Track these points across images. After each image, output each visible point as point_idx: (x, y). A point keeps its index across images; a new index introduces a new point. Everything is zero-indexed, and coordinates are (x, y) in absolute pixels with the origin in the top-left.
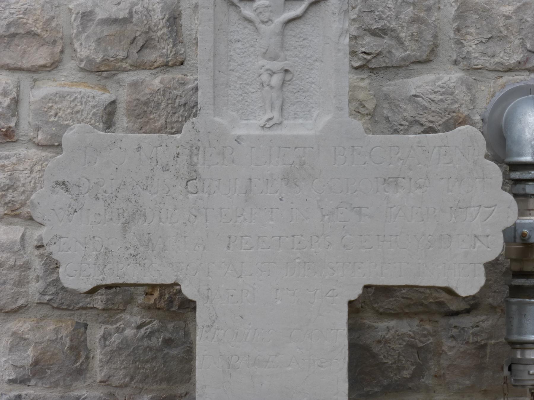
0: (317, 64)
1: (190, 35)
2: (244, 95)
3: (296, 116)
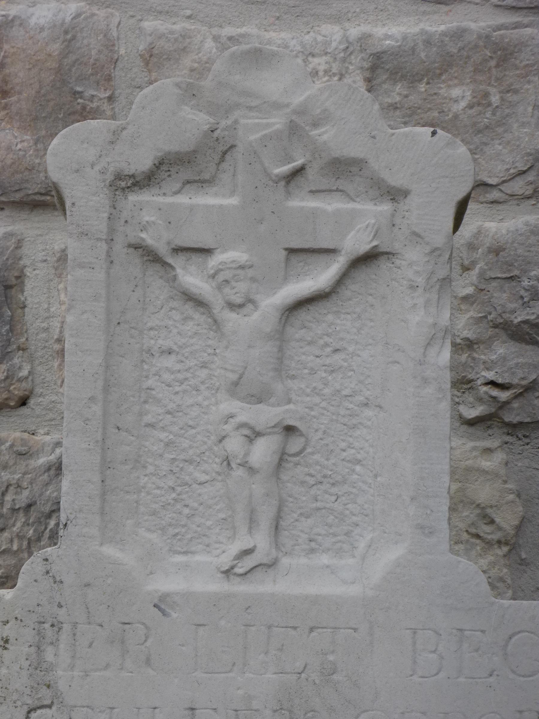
0: (368, 413)
1: (46, 330)
2: (179, 489)
3: (313, 544)
